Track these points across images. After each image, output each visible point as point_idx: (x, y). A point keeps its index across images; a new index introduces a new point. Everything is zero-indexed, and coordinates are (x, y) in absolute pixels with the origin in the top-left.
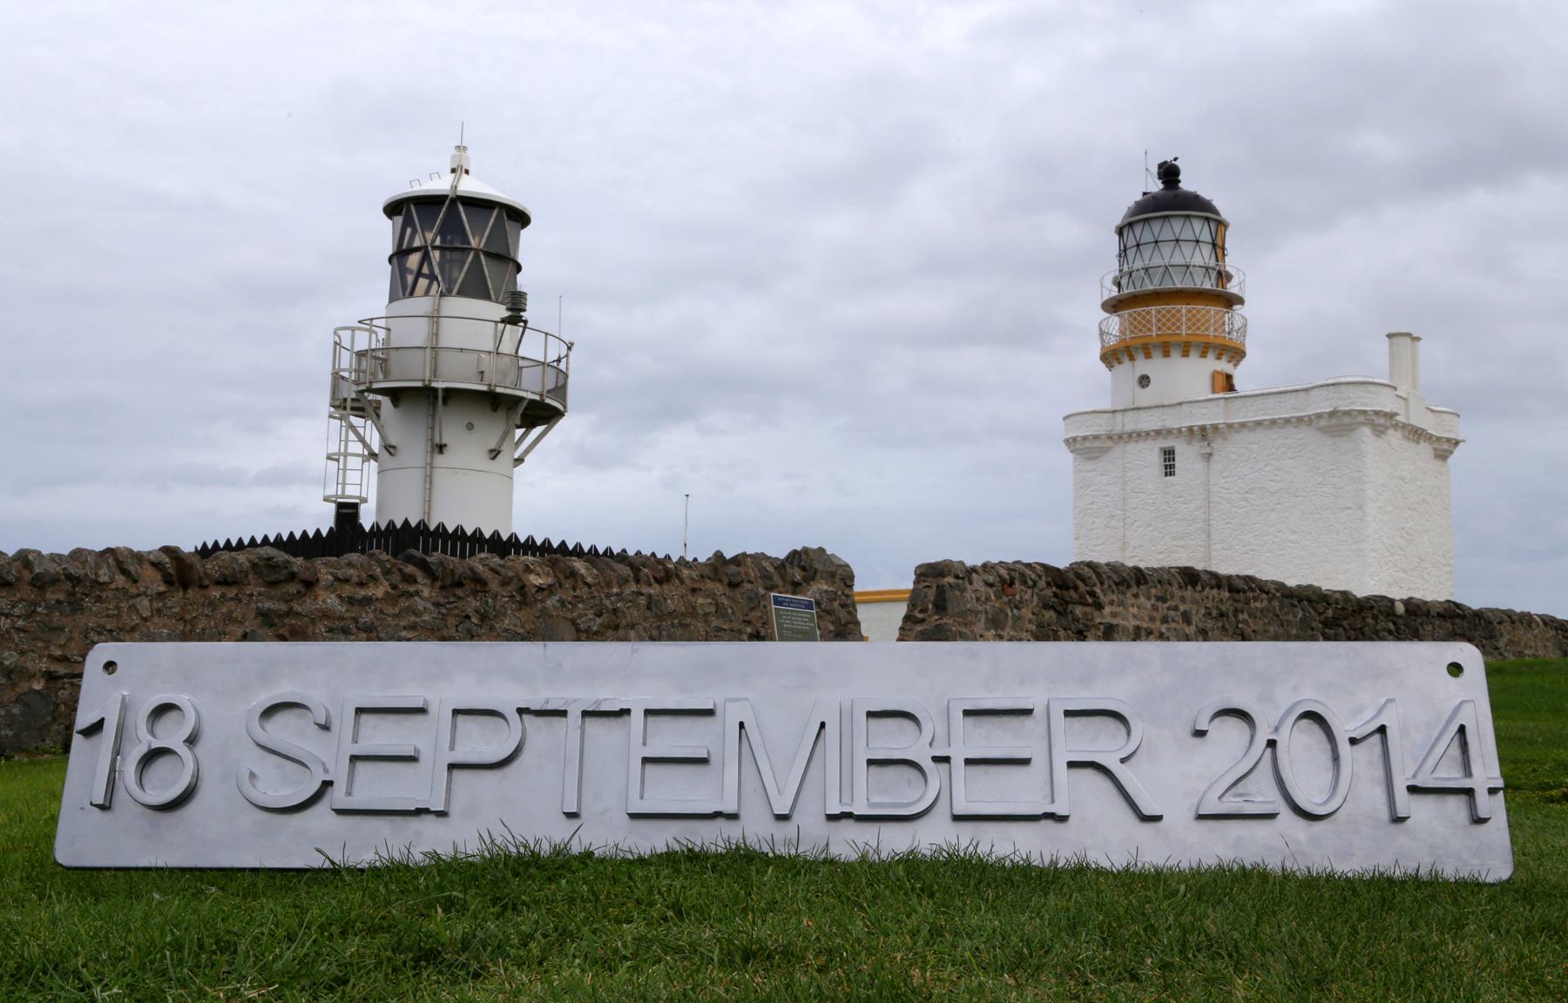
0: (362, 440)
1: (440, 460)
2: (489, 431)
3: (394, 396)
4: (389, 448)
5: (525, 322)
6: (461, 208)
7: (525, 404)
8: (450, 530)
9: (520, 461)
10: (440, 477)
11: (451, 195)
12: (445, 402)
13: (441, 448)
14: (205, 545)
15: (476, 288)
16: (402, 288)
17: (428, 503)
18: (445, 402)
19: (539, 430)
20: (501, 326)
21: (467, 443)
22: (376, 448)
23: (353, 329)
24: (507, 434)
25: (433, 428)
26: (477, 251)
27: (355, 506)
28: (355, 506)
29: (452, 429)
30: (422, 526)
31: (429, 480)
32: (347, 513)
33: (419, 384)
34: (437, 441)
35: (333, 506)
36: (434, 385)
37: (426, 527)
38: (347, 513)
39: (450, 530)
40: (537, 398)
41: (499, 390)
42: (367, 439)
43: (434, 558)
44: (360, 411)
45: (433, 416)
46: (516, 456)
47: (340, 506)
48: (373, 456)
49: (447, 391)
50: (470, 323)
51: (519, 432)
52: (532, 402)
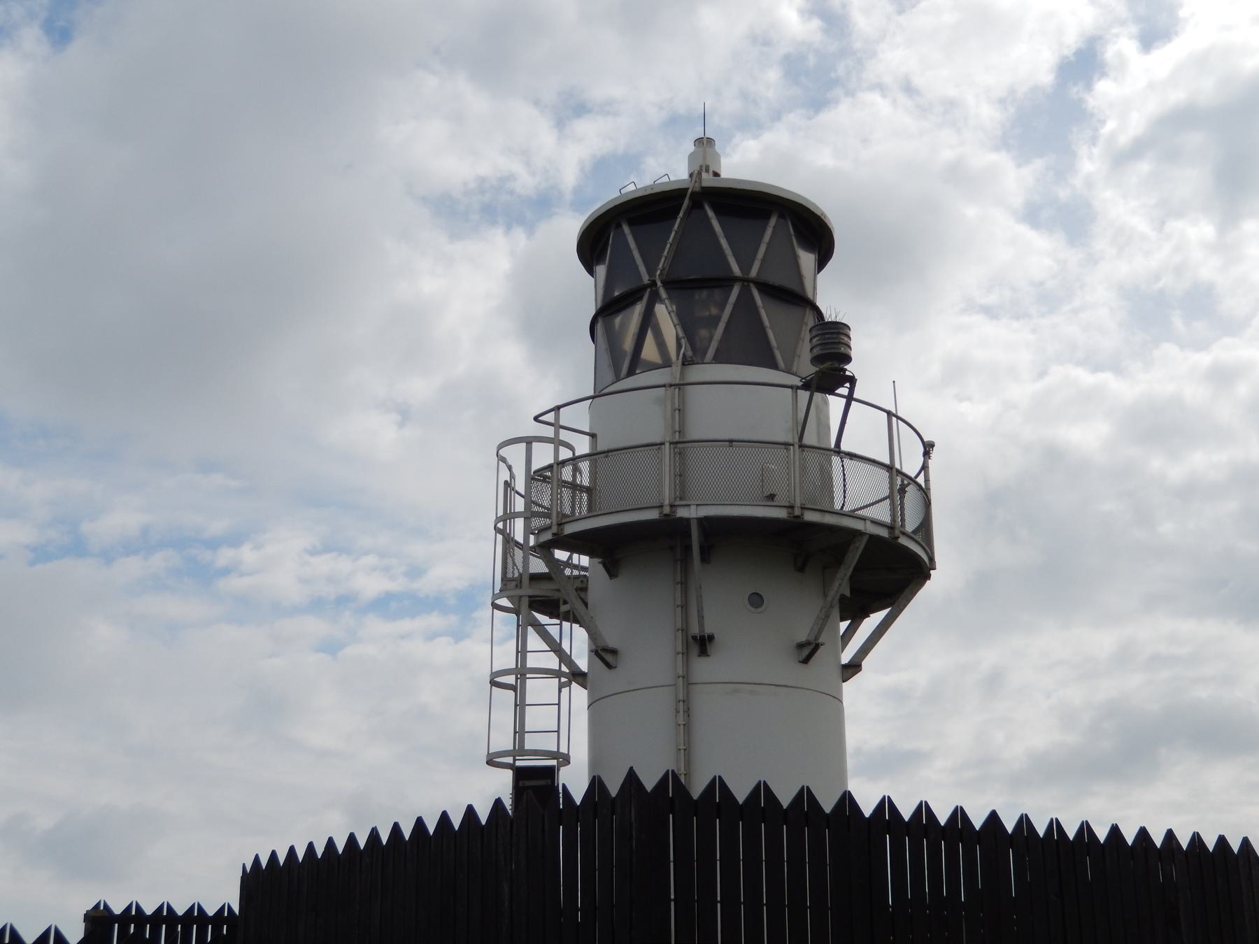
0: (556, 648)
1: (703, 668)
2: (795, 608)
3: (602, 550)
4: (603, 653)
5: (852, 380)
6: (711, 213)
7: (861, 544)
8: (785, 798)
9: (853, 668)
10: (707, 705)
11: (691, 187)
12: (705, 557)
13: (703, 644)
14: (257, 860)
15: (751, 347)
16: (619, 363)
17: (687, 751)
18: (705, 557)
19: (876, 618)
20: (804, 395)
21: (752, 626)
22: (583, 663)
23: (529, 441)
24: (823, 622)
25: (685, 607)
26: (745, 281)
27: (550, 773)
28: (550, 773)
29: (721, 599)
30: (672, 785)
31: (685, 707)
32: (535, 783)
33: (653, 515)
34: (695, 630)
35: (508, 775)
36: (682, 513)
37: (681, 790)
38: (535, 783)
39: (785, 798)
40: (884, 533)
41: (810, 517)
42: (565, 646)
43: (541, 510)
44: (551, 607)
45: (684, 584)
46: (846, 657)
47: (521, 775)
48: (577, 676)
49: (708, 524)
50: (740, 404)
51: (844, 625)
52: (874, 539)
